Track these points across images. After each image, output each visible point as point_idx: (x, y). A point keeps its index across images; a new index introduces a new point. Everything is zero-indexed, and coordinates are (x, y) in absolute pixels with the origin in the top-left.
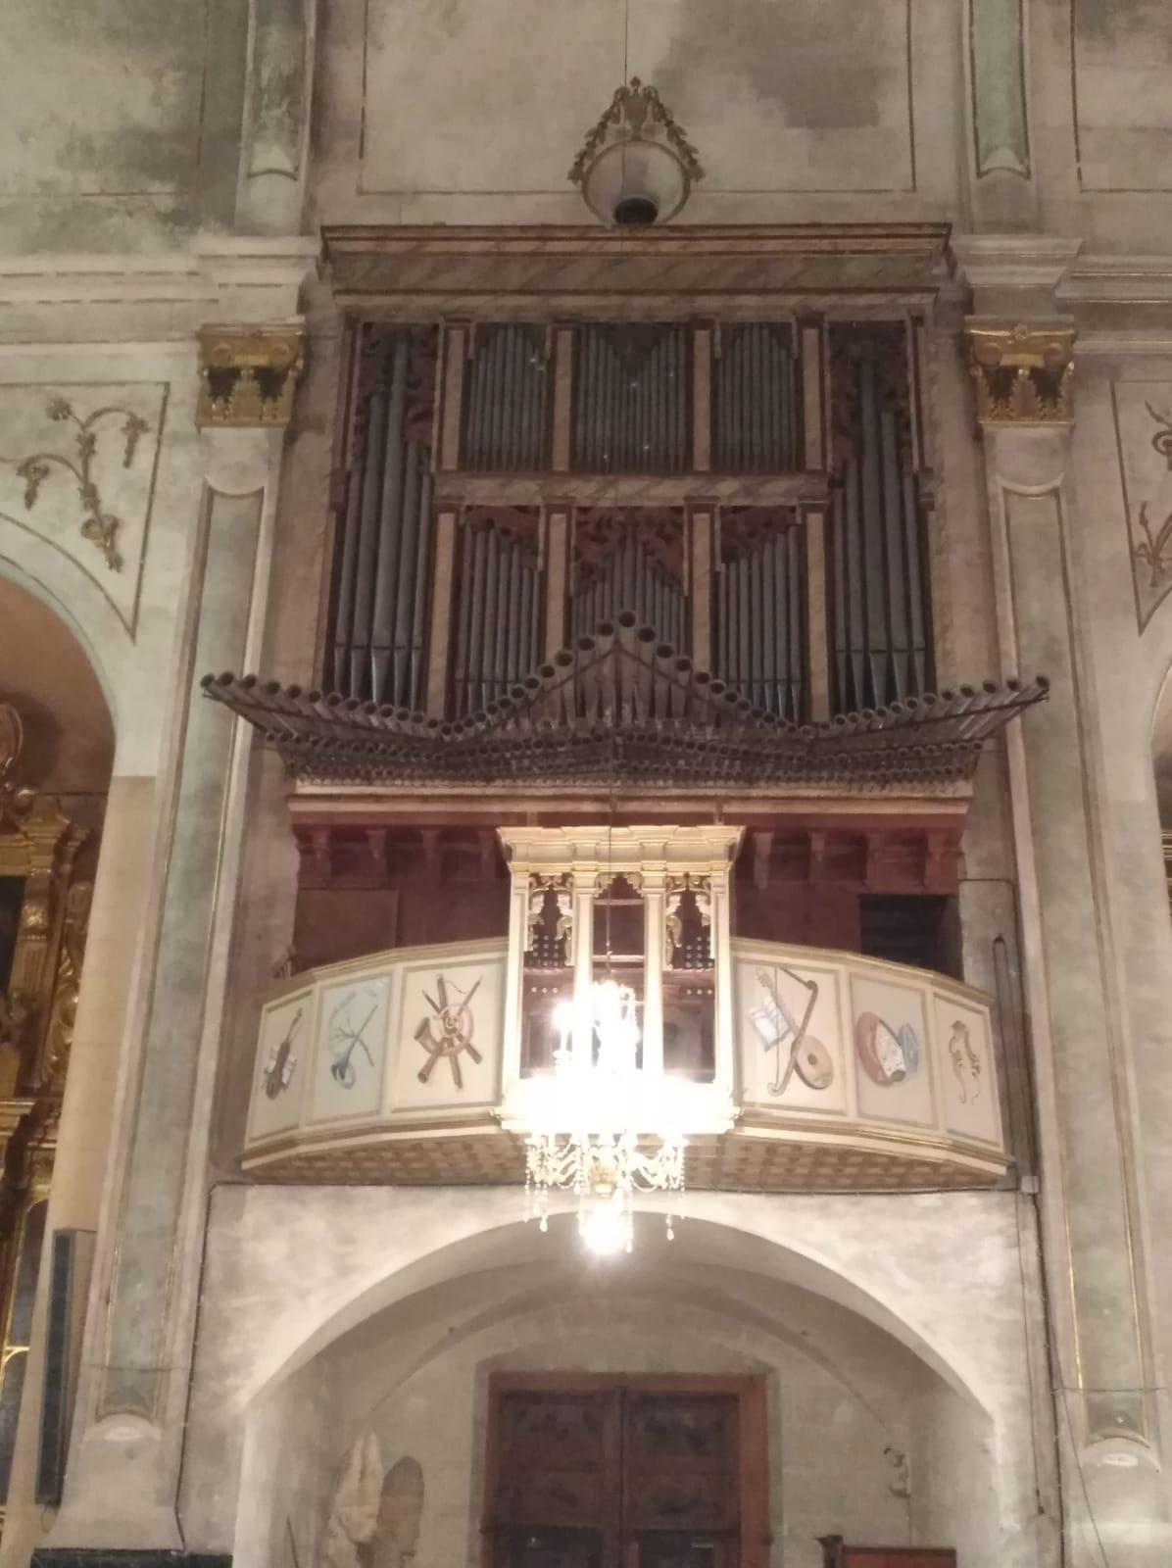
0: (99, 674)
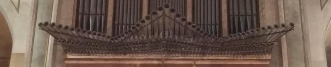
0: (8, 22)
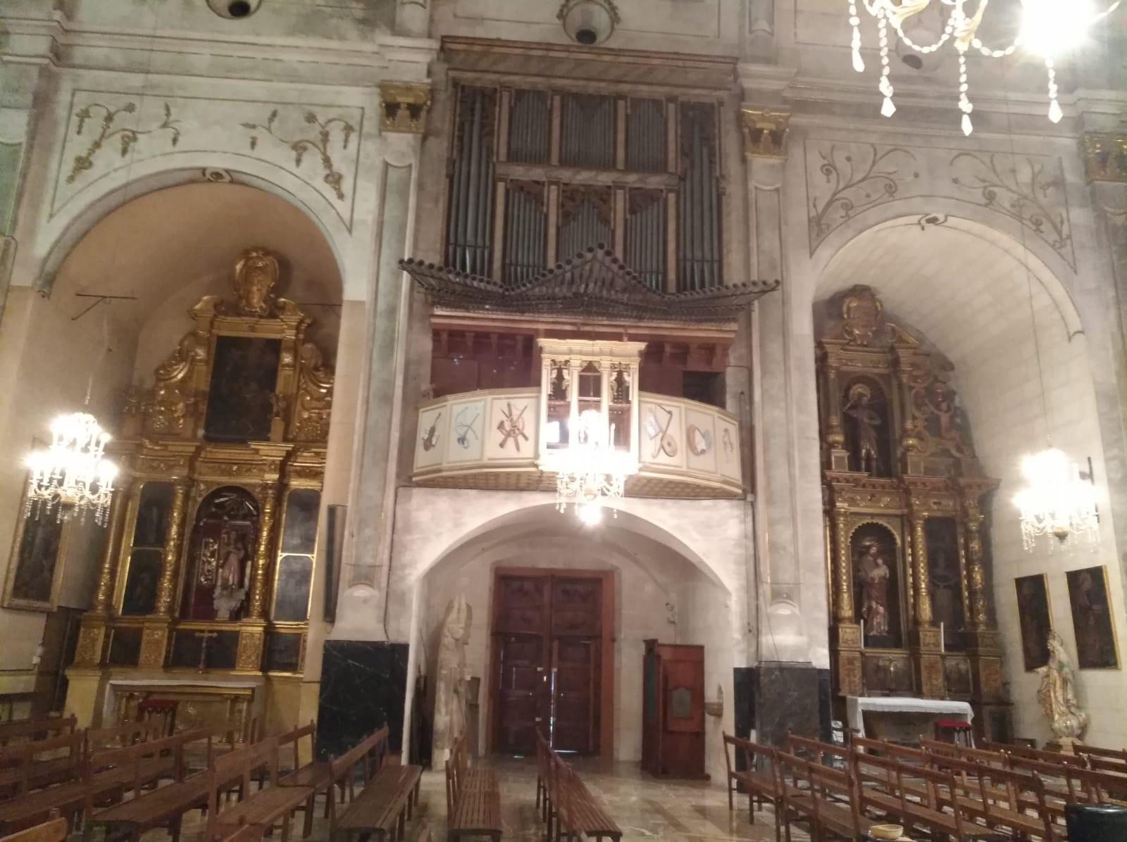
0: (334, 249)
